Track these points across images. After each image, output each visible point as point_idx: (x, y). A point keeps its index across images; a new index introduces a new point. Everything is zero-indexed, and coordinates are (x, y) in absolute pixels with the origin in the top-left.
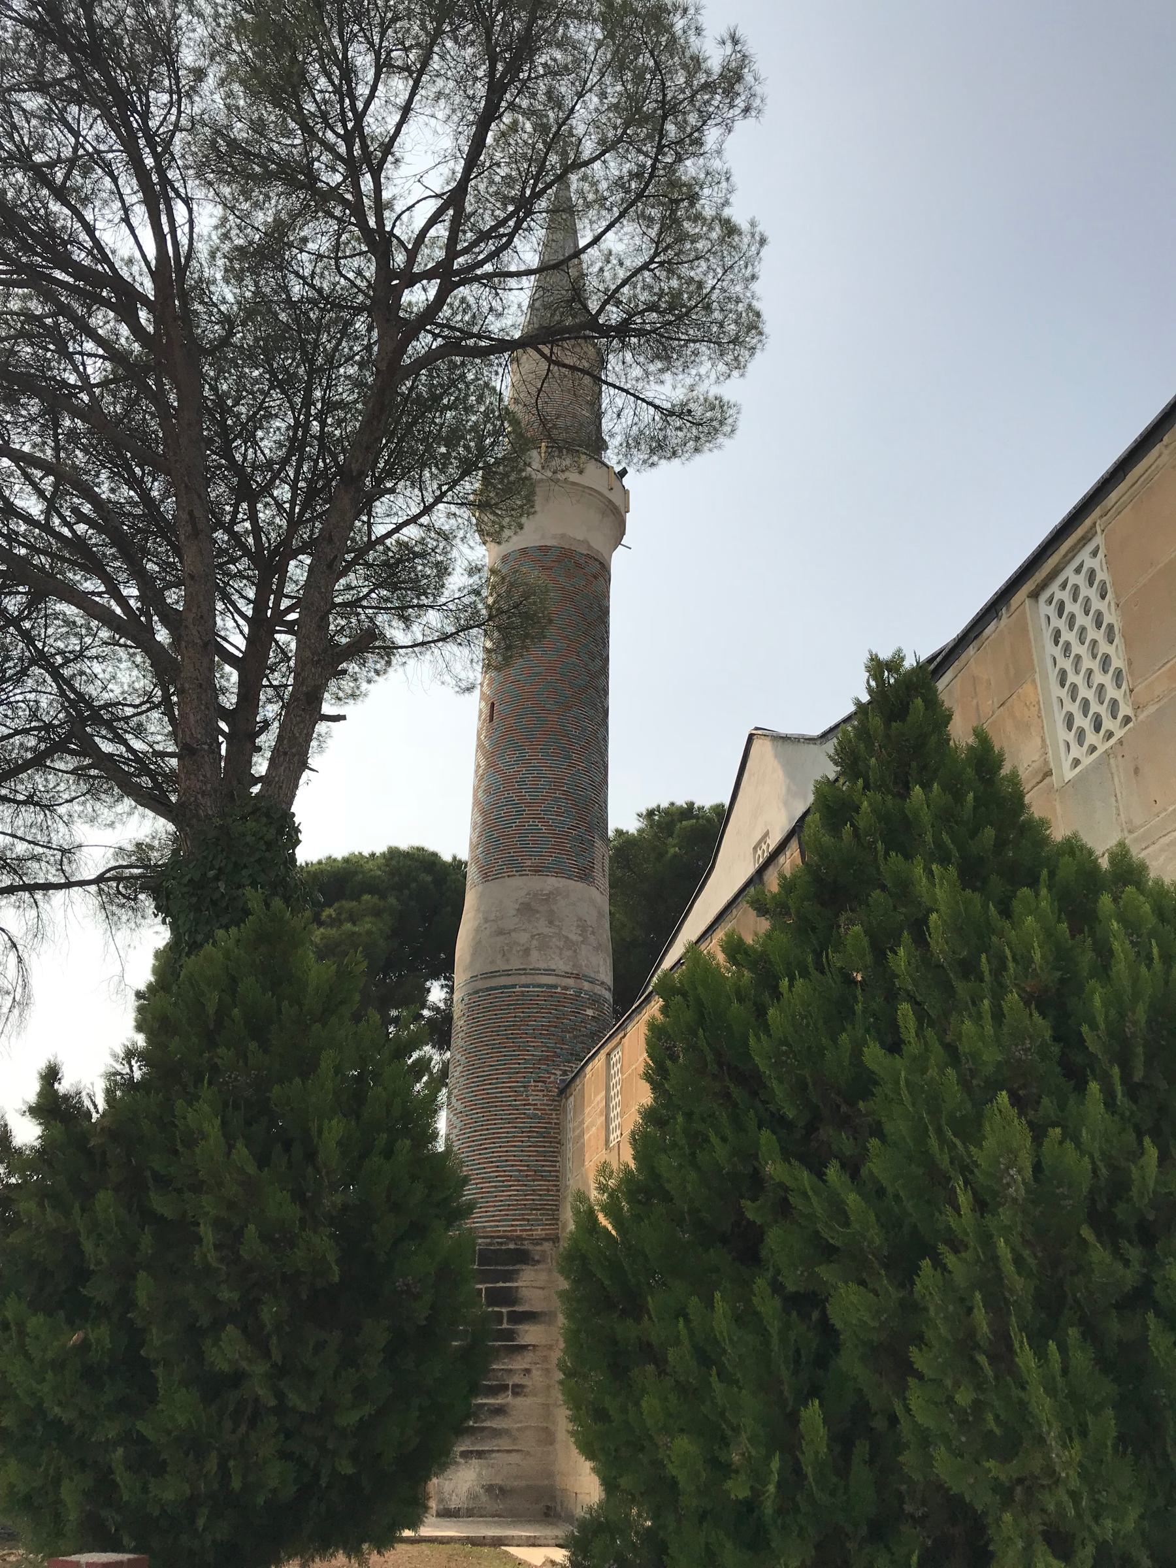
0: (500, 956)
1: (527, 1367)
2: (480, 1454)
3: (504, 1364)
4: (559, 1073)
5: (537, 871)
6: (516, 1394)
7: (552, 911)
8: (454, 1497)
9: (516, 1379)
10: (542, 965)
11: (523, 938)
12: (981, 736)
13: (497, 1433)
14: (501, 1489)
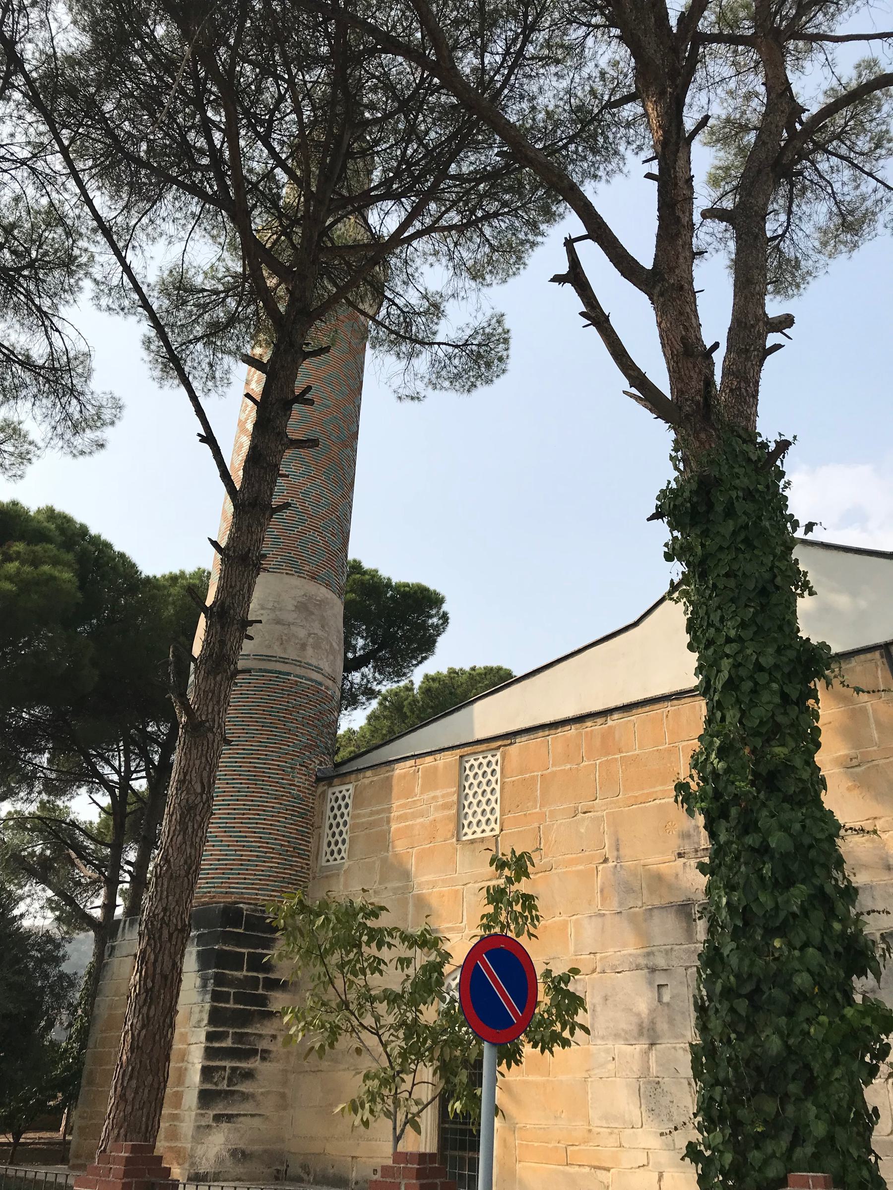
0: (278, 643)
1: (274, 1033)
2: (229, 1118)
3: (256, 1028)
4: (317, 762)
5: (313, 578)
6: (263, 1059)
7: (323, 617)
8: (204, 1161)
9: (263, 1045)
10: (314, 662)
11: (302, 633)
12: (668, 557)
13: (246, 1097)
14: (243, 1153)
